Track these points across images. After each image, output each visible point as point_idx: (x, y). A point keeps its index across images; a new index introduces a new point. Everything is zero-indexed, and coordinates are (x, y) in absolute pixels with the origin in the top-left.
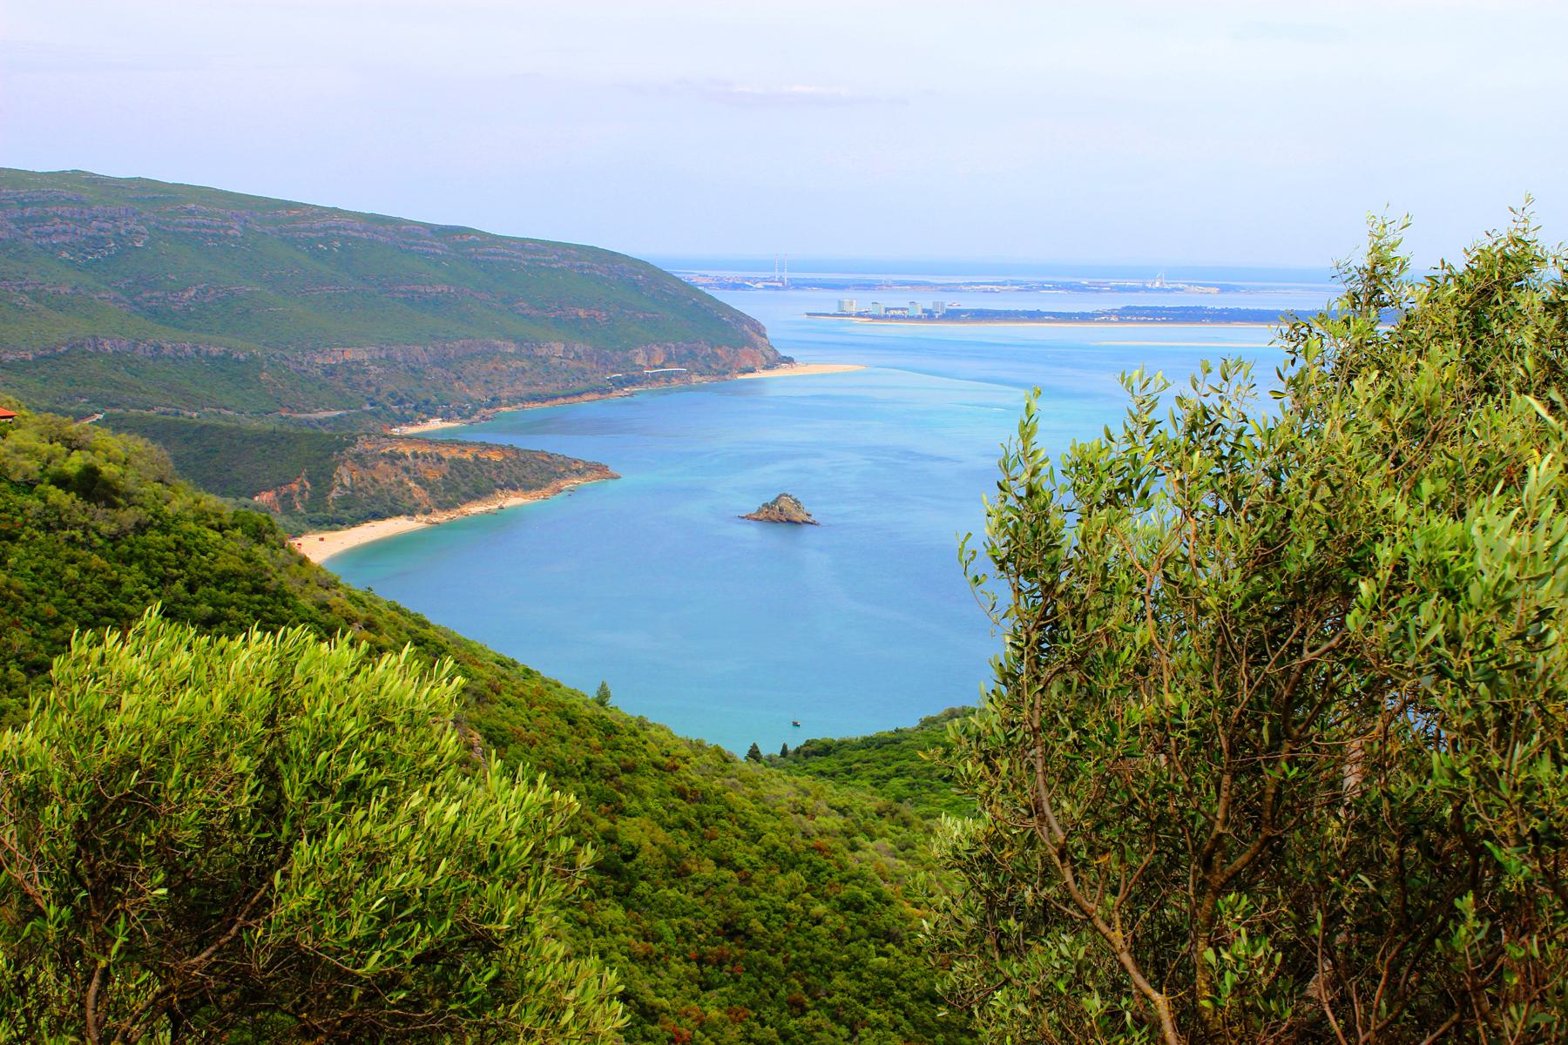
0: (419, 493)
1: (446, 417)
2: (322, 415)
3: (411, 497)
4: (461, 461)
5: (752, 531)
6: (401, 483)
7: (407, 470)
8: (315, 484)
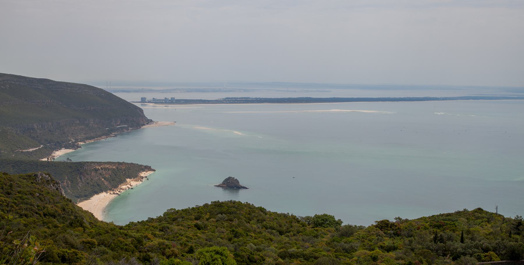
0: (106, 183)
1: (67, 147)
2: (31, 150)
3: (104, 184)
4: (114, 169)
5: (221, 189)
6: (99, 179)
7: (100, 174)
8: (72, 182)
